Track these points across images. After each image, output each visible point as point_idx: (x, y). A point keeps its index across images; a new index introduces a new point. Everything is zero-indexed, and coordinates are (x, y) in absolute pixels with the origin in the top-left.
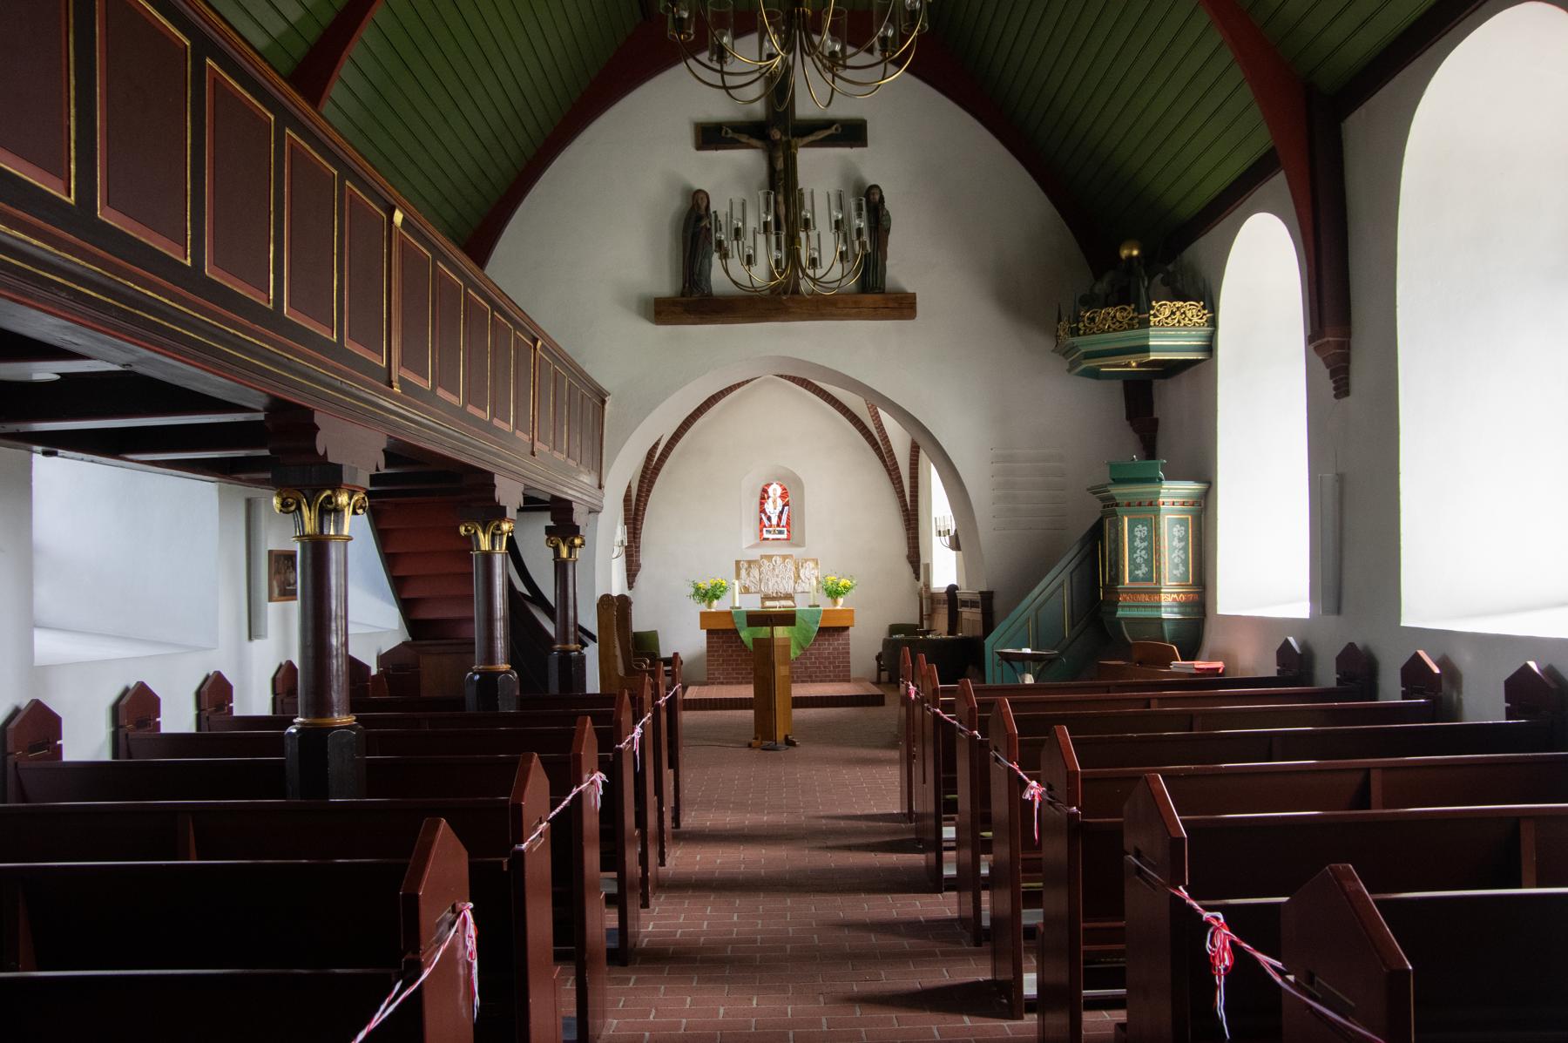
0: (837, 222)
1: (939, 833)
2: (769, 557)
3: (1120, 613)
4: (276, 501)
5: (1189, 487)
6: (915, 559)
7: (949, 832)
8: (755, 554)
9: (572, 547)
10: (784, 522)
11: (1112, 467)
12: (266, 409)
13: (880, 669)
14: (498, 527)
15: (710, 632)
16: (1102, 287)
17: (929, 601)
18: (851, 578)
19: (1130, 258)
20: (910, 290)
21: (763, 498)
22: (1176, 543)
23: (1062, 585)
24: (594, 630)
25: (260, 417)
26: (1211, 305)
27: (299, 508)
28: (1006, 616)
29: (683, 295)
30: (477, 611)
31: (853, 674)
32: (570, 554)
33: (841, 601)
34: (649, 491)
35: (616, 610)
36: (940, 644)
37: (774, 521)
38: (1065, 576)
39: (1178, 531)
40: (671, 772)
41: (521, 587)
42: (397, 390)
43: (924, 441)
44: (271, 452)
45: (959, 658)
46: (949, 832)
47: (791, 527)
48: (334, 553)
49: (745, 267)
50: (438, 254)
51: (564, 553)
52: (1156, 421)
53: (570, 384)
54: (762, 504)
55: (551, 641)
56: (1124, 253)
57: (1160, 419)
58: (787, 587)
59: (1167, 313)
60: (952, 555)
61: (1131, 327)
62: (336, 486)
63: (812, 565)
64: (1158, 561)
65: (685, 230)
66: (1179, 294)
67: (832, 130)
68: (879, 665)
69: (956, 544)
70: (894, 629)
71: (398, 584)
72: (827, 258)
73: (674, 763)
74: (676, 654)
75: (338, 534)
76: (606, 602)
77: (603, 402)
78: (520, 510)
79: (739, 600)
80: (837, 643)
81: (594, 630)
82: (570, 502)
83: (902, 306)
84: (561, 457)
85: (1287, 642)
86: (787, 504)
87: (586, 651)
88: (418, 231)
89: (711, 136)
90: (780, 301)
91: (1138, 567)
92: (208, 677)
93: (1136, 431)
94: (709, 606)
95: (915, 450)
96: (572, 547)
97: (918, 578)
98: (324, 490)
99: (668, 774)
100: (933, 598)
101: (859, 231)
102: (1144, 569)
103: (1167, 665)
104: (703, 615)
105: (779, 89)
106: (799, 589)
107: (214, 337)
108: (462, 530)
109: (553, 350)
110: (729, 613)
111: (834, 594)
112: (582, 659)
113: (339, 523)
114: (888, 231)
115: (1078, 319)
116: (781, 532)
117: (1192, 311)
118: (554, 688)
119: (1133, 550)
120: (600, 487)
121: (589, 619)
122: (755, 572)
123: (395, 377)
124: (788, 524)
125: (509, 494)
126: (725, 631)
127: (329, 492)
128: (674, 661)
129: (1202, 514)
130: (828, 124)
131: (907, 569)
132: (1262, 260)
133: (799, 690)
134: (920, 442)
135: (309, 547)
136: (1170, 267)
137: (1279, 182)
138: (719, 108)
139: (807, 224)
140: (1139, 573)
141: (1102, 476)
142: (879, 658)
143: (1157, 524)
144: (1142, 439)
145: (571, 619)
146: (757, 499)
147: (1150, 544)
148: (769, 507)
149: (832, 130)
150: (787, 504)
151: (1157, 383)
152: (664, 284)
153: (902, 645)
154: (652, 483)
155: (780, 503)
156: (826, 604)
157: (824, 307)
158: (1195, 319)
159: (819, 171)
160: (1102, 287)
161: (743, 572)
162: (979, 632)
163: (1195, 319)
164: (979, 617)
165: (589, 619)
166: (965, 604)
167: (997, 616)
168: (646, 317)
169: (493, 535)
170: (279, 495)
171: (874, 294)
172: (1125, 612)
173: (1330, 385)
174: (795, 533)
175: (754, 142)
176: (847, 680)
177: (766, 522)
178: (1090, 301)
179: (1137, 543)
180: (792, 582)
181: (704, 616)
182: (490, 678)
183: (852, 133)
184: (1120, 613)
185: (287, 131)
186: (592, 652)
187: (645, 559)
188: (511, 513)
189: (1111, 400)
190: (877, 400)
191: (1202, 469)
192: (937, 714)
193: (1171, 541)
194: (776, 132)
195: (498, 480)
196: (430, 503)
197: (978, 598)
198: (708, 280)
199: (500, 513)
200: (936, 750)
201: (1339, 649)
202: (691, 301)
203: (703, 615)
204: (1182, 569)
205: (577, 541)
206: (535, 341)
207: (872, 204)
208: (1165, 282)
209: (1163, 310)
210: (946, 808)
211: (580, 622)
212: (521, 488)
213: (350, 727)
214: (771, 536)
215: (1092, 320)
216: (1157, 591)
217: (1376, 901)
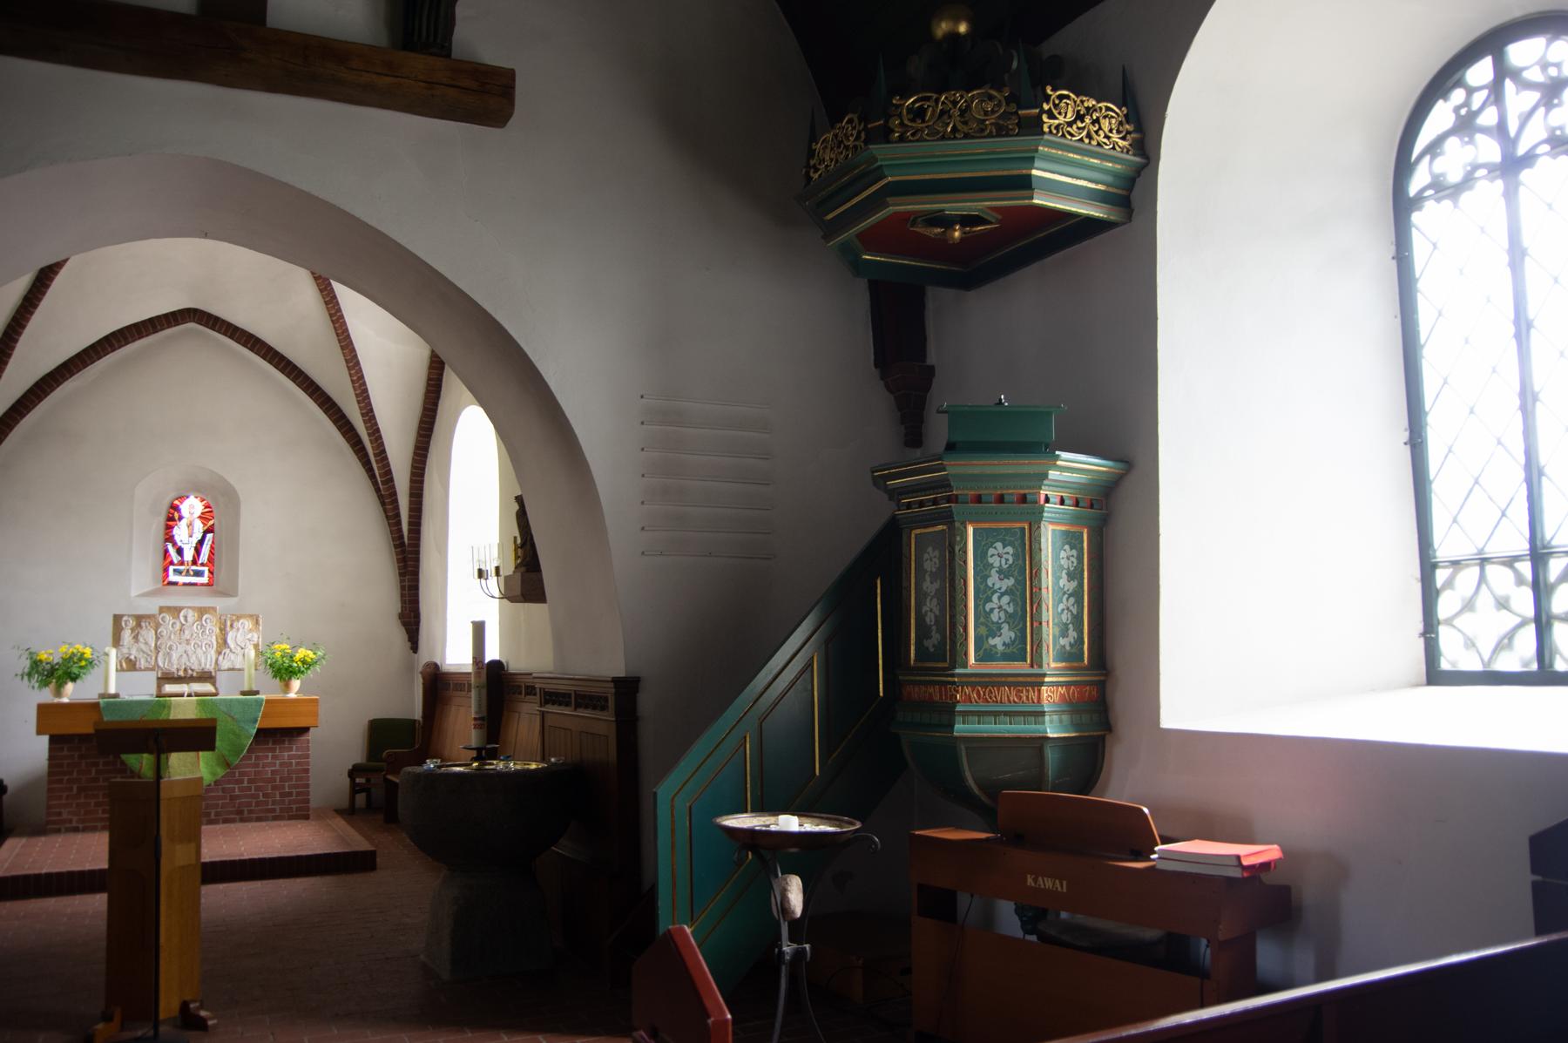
2: (175, 611)
3: (961, 728)
6: (411, 618)
8: (150, 606)
10: (204, 557)
13: (355, 789)
15: (55, 741)
18: (314, 647)
19: (954, 36)
21: (170, 519)
22: (1063, 582)
31: (315, 801)
33: (296, 684)
39: (1066, 556)
47: (217, 563)
54: (169, 528)
58: (204, 659)
59: (1070, 117)
61: (1001, 131)
68: (353, 784)
79: (114, 681)
80: (288, 754)
83: (484, 97)
86: (210, 530)
91: (994, 631)
94: (58, 693)
97: (415, 646)
100: (438, 683)
102: (1007, 634)
103: (1143, 852)
104: (43, 710)
106: (225, 664)
110: (95, 706)
111: (284, 672)
116: (198, 574)
119: (984, 594)
122: (148, 635)
124: (211, 559)
129: (1118, 526)
131: (398, 635)
133: (221, 844)
140: (997, 642)
142: (354, 772)
146: (162, 519)
148: (180, 533)
150: (210, 530)
153: (393, 743)
155: (199, 527)
156: (270, 691)
161: (127, 635)
163: (1115, 137)
174: (221, 576)
177: (175, 557)
179: (993, 580)
180: (212, 653)
181: (46, 713)
184: (961, 728)
193: (1057, 578)
203: (43, 710)
204: (1072, 634)
209: (1062, 109)
216: (1037, 682)
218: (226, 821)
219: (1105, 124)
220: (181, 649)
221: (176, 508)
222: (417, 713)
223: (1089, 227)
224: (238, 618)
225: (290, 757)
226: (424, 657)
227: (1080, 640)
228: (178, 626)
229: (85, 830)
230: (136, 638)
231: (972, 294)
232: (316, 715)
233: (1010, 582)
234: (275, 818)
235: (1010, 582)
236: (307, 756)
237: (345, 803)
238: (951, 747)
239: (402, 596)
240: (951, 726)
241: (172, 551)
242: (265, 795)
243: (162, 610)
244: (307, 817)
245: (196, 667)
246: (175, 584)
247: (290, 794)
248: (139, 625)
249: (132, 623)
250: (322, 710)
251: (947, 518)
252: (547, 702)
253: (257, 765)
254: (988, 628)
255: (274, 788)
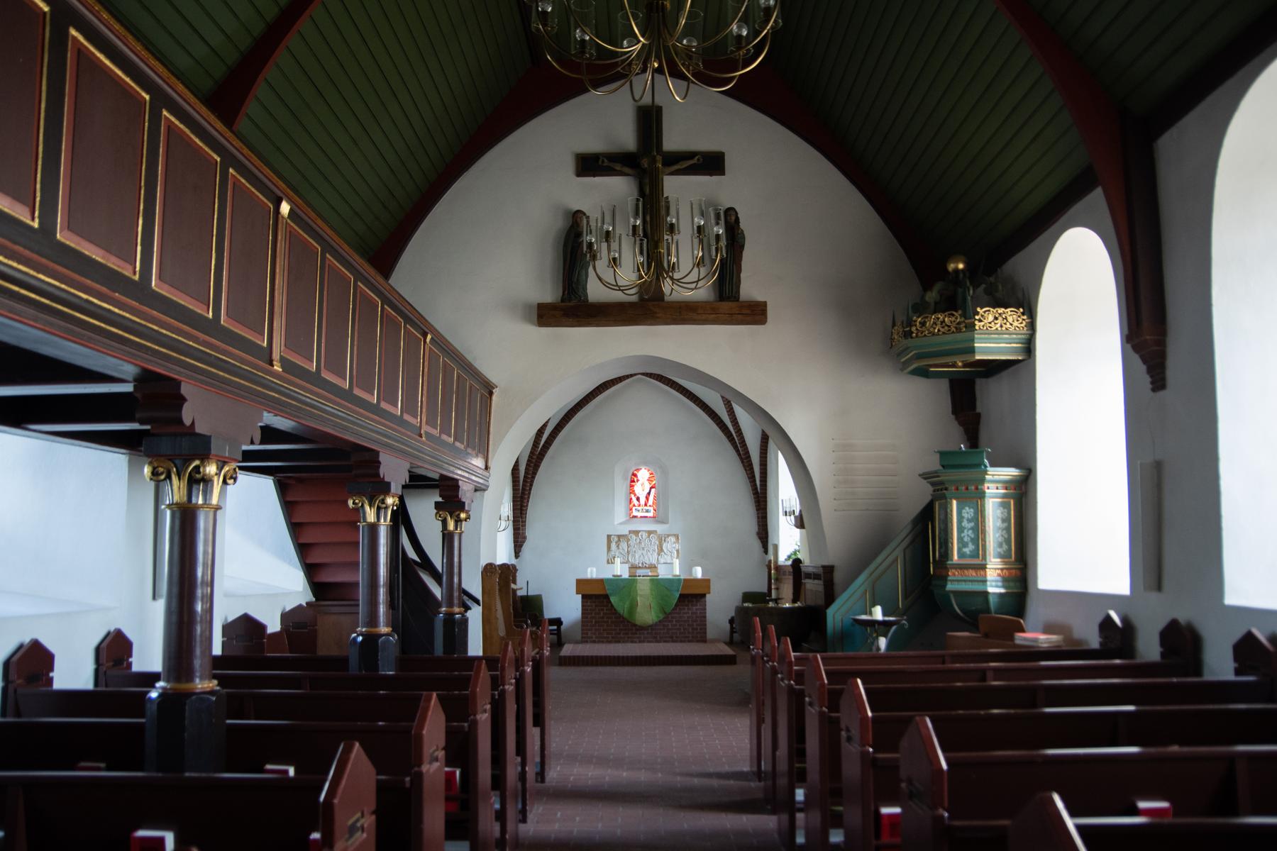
0: (699, 227)
1: (793, 794)
3: (950, 587)
4: (147, 470)
5: (1010, 473)
6: (764, 534)
7: (800, 794)
8: (624, 530)
9: (458, 521)
10: (650, 502)
11: (943, 454)
12: (135, 380)
13: (732, 631)
14: (383, 501)
15: (584, 597)
16: (932, 296)
17: (775, 573)
19: (957, 271)
20: (760, 298)
23: (896, 560)
24: (478, 594)
25: (128, 388)
26: (1030, 312)
27: (169, 477)
28: (844, 590)
29: (562, 301)
30: (361, 577)
31: (710, 634)
34: (533, 477)
35: (500, 577)
36: (792, 615)
38: (898, 553)
40: (537, 731)
41: (412, 554)
42: (277, 368)
43: (773, 434)
44: (151, 425)
45: (806, 625)
46: (800, 794)
48: (202, 523)
49: (618, 273)
50: (327, 247)
51: (451, 526)
52: (979, 415)
53: (458, 376)
55: (439, 605)
56: (951, 267)
57: (984, 412)
59: (991, 318)
60: (797, 532)
61: (959, 330)
62: (205, 457)
63: (673, 539)
64: (984, 540)
65: (565, 245)
66: (998, 302)
67: (695, 161)
68: (732, 628)
69: (800, 523)
70: (747, 597)
71: (303, 549)
72: (689, 278)
73: (539, 721)
74: (926, 476)
75: (206, 503)
76: (489, 570)
77: (491, 394)
78: (404, 487)
81: (478, 594)
82: (457, 480)
83: (755, 313)
84: (461, 446)
85: (1108, 619)
87: (469, 614)
88: (307, 223)
89: (589, 165)
90: (648, 307)
91: (965, 545)
92: (109, 633)
93: (961, 423)
95: (765, 439)
96: (458, 521)
97: (766, 552)
98: (194, 460)
99: (533, 733)
101: (718, 236)
105: (649, 120)
106: (662, 561)
108: (350, 503)
109: (442, 344)
112: (465, 622)
113: (207, 493)
114: (742, 247)
115: (910, 323)
117: (1013, 319)
118: (439, 649)
119: (961, 530)
120: (487, 468)
121: (473, 584)
122: (624, 545)
123: (276, 356)
125: (394, 470)
127: (197, 462)
128: (558, 622)
129: (1022, 495)
130: (691, 155)
131: (757, 544)
132: (1079, 272)
134: (769, 432)
135: (178, 515)
136: (992, 279)
137: (1096, 198)
138: (594, 145)
139: (672, 228)
140: (967, 550)
141: (934, 464)
143: (983, 506)
144: (967, 431)
145: (456, 586)
147: (977, 524)
149: (695, 161)
151: (979, 382)
152: (548, 293)
154: (537, 467)
157: (685, 313)
158: (1016, 324)
159: (678, 188)
160: (932, 296)
161: (613, 546)
162: (821, 602)
163: (1016, 324)
164: (821, 588)
165: (473, 584)
166: (808, 576)
167: (837, 588)
168: (531, 322)
169: (379, 508)
170: (150, 463)
171: (730, 304)
172: (954, 584)
173: (1148, 379)
175: (626, 170)
176: (702, 638)
178: (920, 308)
179: (965, 524)
182: (372, 639)
183: (712, 164)
184: (950, 587)
185: (231, 170)
186: (475, 616)
187: (531, 532)
188: (396, 488)
189: (934, 395)
190: (731, 397)
191: (1022, 457)
192: (790, 686)
194: (646, 161)
195: (382, 458)
196: (320, 477)
197: (820, 571)
198: (585, 289)
199: (385, 488)
200: (784, 709)
201: (1161, 624)
202: (569, 307)
204: (1005, 547)
205: (463, 516)
206: (425, 335)
207: (731, 220)
208: (987, 292)
210: (799, 777)
211: (464, 586)
212: (408, 466)
213: (212, 692)
214: (639, 514)
215: (923, 324)
219: (1010, 319)
221: (635, 475)
223: (1017, 362)
227: (1010, 549)
231: (990, 380)
233: (972, 524)
235: (972, 524)
237: (728, 640)
238: (947, 595)
240: (945, 586)
241: (634, 499)
250: (714, 587)
251: (944, 497)
254: (962, 544)
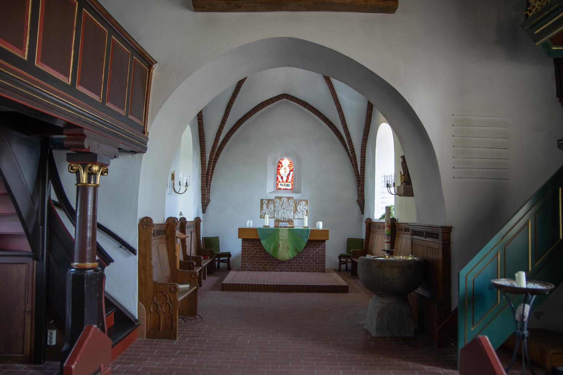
6: (362, 200)
8: (272, 197)
13: (341, 263)
15: (244, 240)
23: (527, 224)
32: (89, 180)
37: (285, 179)
54: (278, 170)
58: (290, 215)
63: (304, 203)
68: (340, 261)
96: (91, 174)
97: (363, 212)
100: (370, 225)
106: (296, 217)
107: (119, 132)
116: (288, 185)
122: (271, 206)
126: (252, 240)
131: (357, 208)
142: (341, 257)
148: (282, 171)
185: (84, 9)
214: (283, 187)
217: (22, 48)
218: (297, 271)
220: (282, 211)
222: (364, 237)
224: (301, 201)
225: (319, 250)
226: (366, 216)
228: (281, 203)
229: (253, 270)
230: (268, 207)
232: (328, 236)
234: (314, 271)
236: (325, 250)
237: (337, 268)
239: (358, 194)
242: (310, 263)
243: (276, 197)
244: (324, 272)
245: (287, 217)
246: (280, 189)
247: (319, 263)
248: (268, 203)
249: (266, 202)
252: (414, 235)
253: (307, 252)
255: (313, 261)
